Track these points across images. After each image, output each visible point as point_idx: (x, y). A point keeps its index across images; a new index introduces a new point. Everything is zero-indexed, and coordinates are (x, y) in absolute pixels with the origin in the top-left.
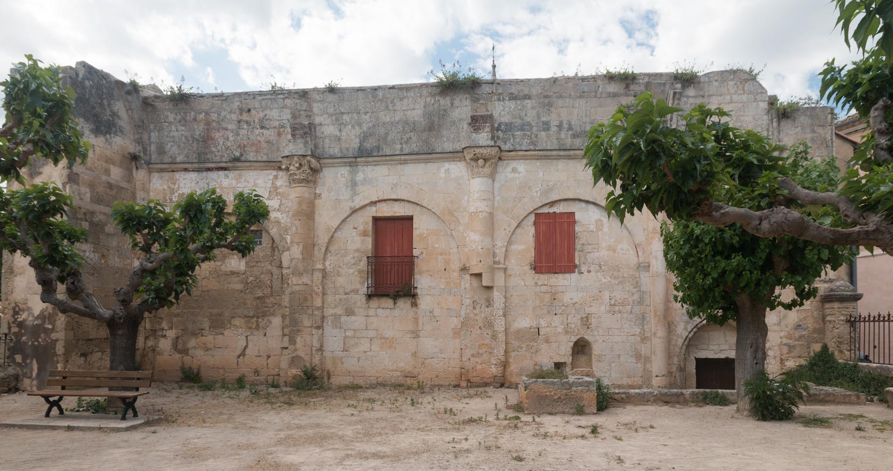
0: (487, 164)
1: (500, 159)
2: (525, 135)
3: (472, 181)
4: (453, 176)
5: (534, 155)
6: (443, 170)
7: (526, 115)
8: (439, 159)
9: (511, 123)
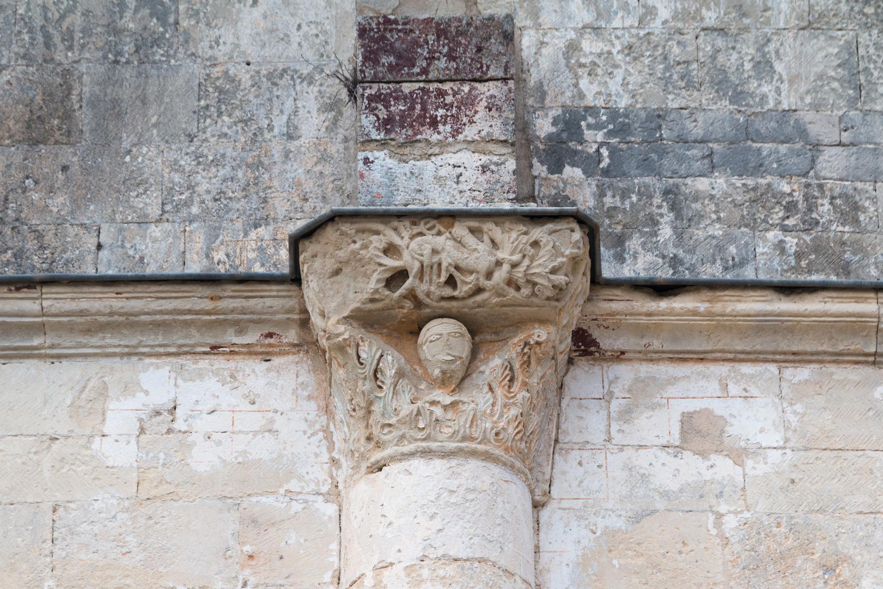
0: (493, 365)
1: (584, 344)
2: (761, 198)
3: (363, 491)
4: (204, 458)
5: (854, 326)
6: (121, 414)
7: (764, 66)
8: (96, 326)
9: (659, 117)
